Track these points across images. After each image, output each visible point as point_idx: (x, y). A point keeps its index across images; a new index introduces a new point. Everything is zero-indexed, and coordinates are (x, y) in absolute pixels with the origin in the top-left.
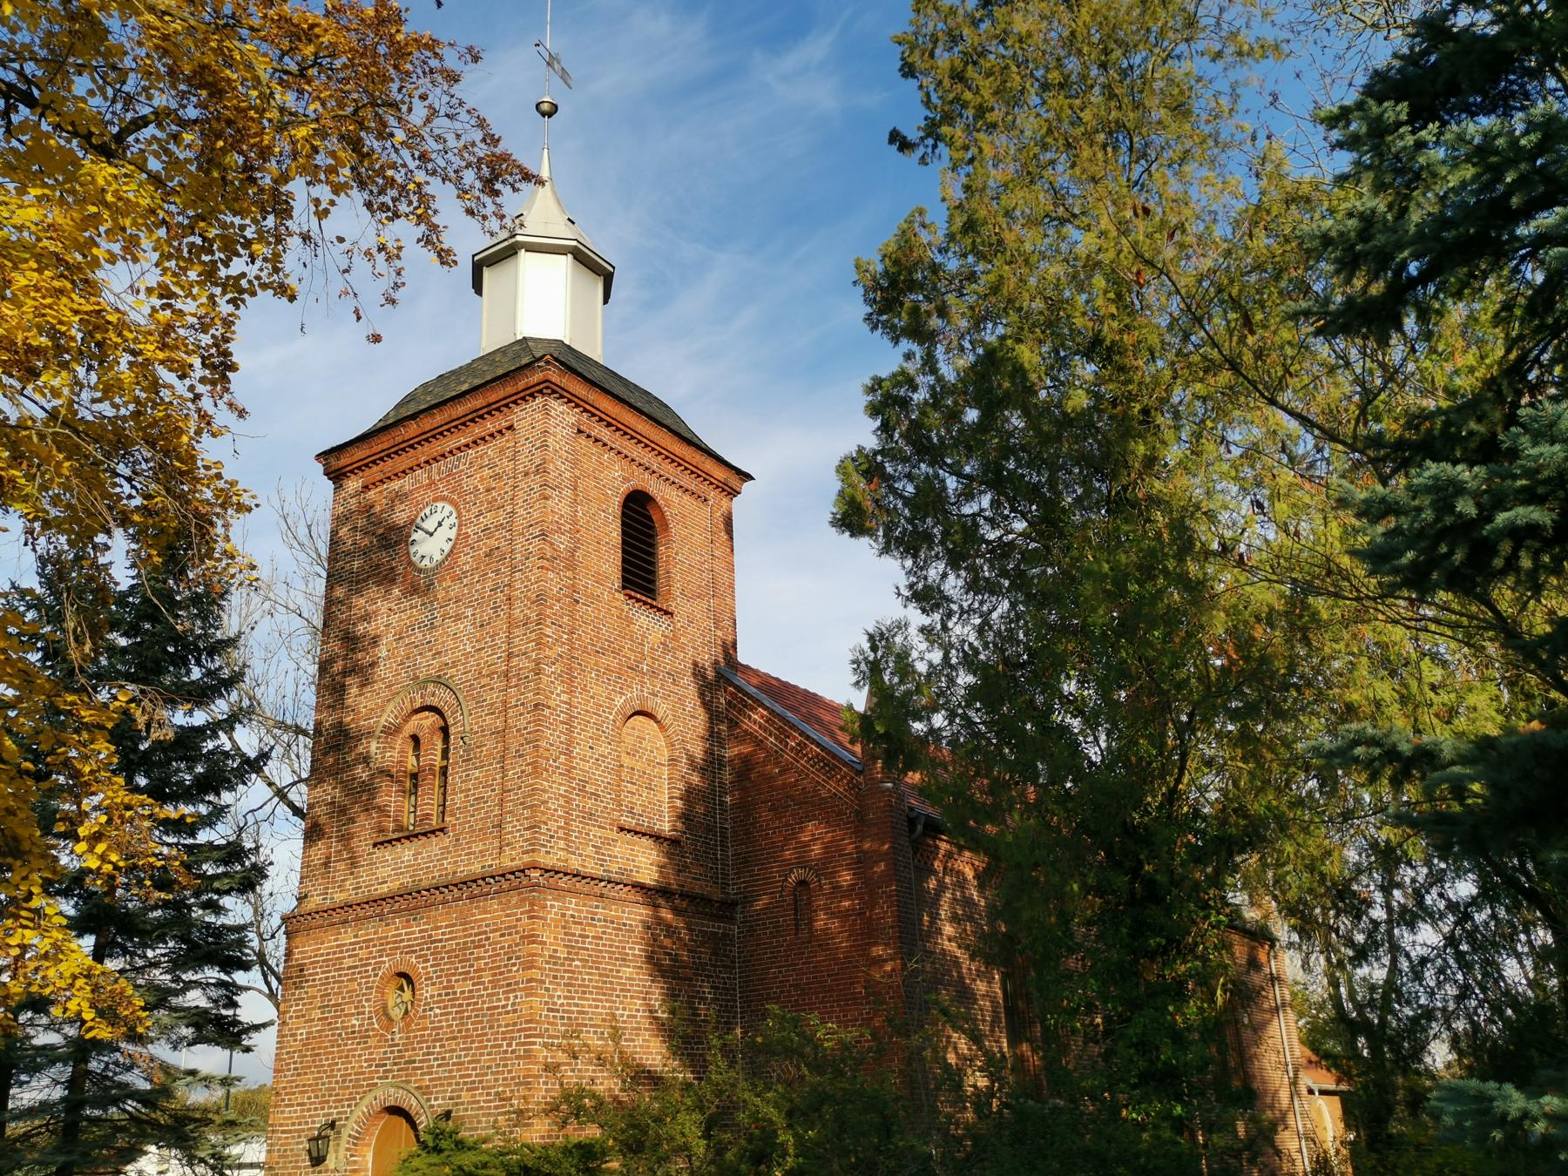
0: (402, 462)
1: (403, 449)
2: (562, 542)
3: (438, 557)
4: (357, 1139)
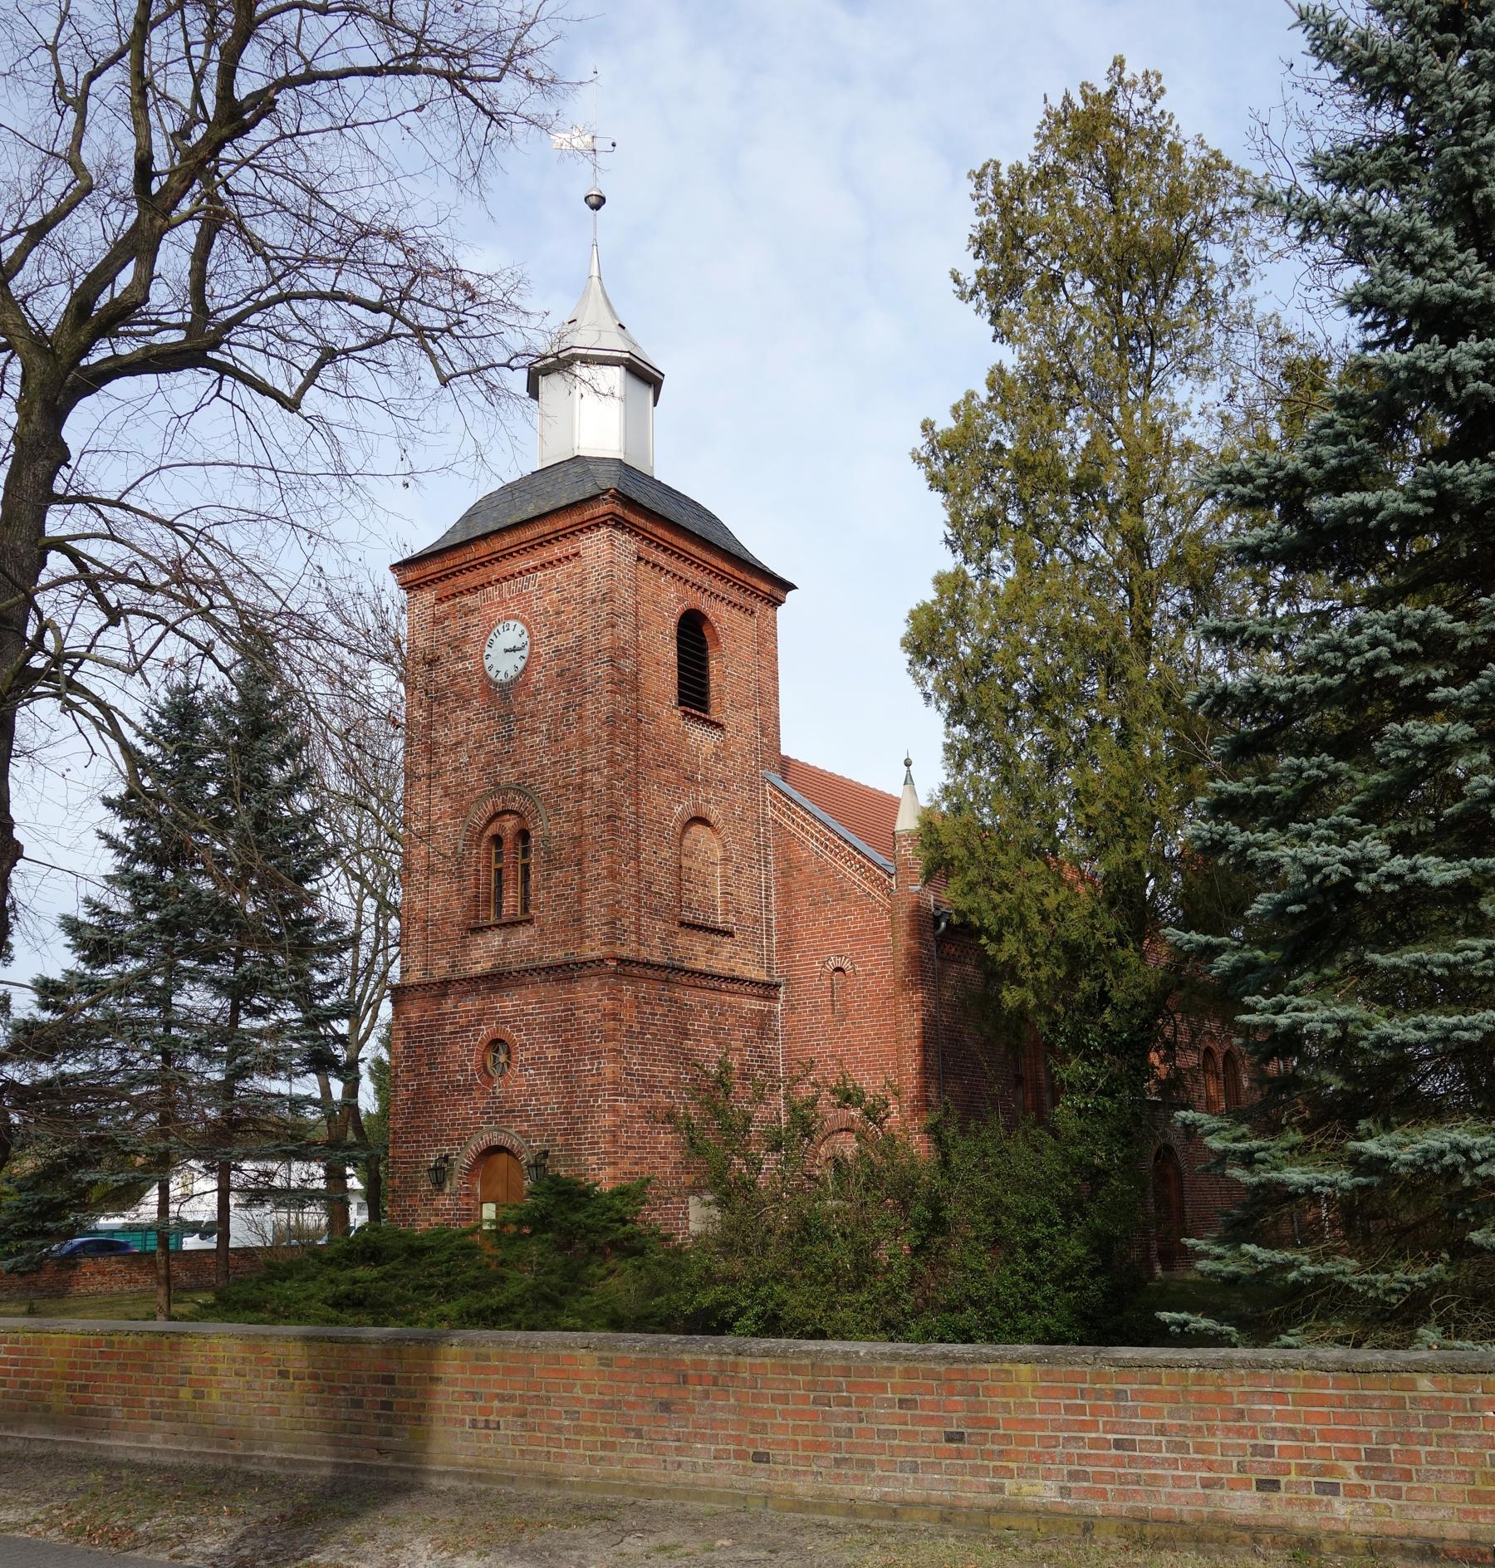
1: (474, 566)
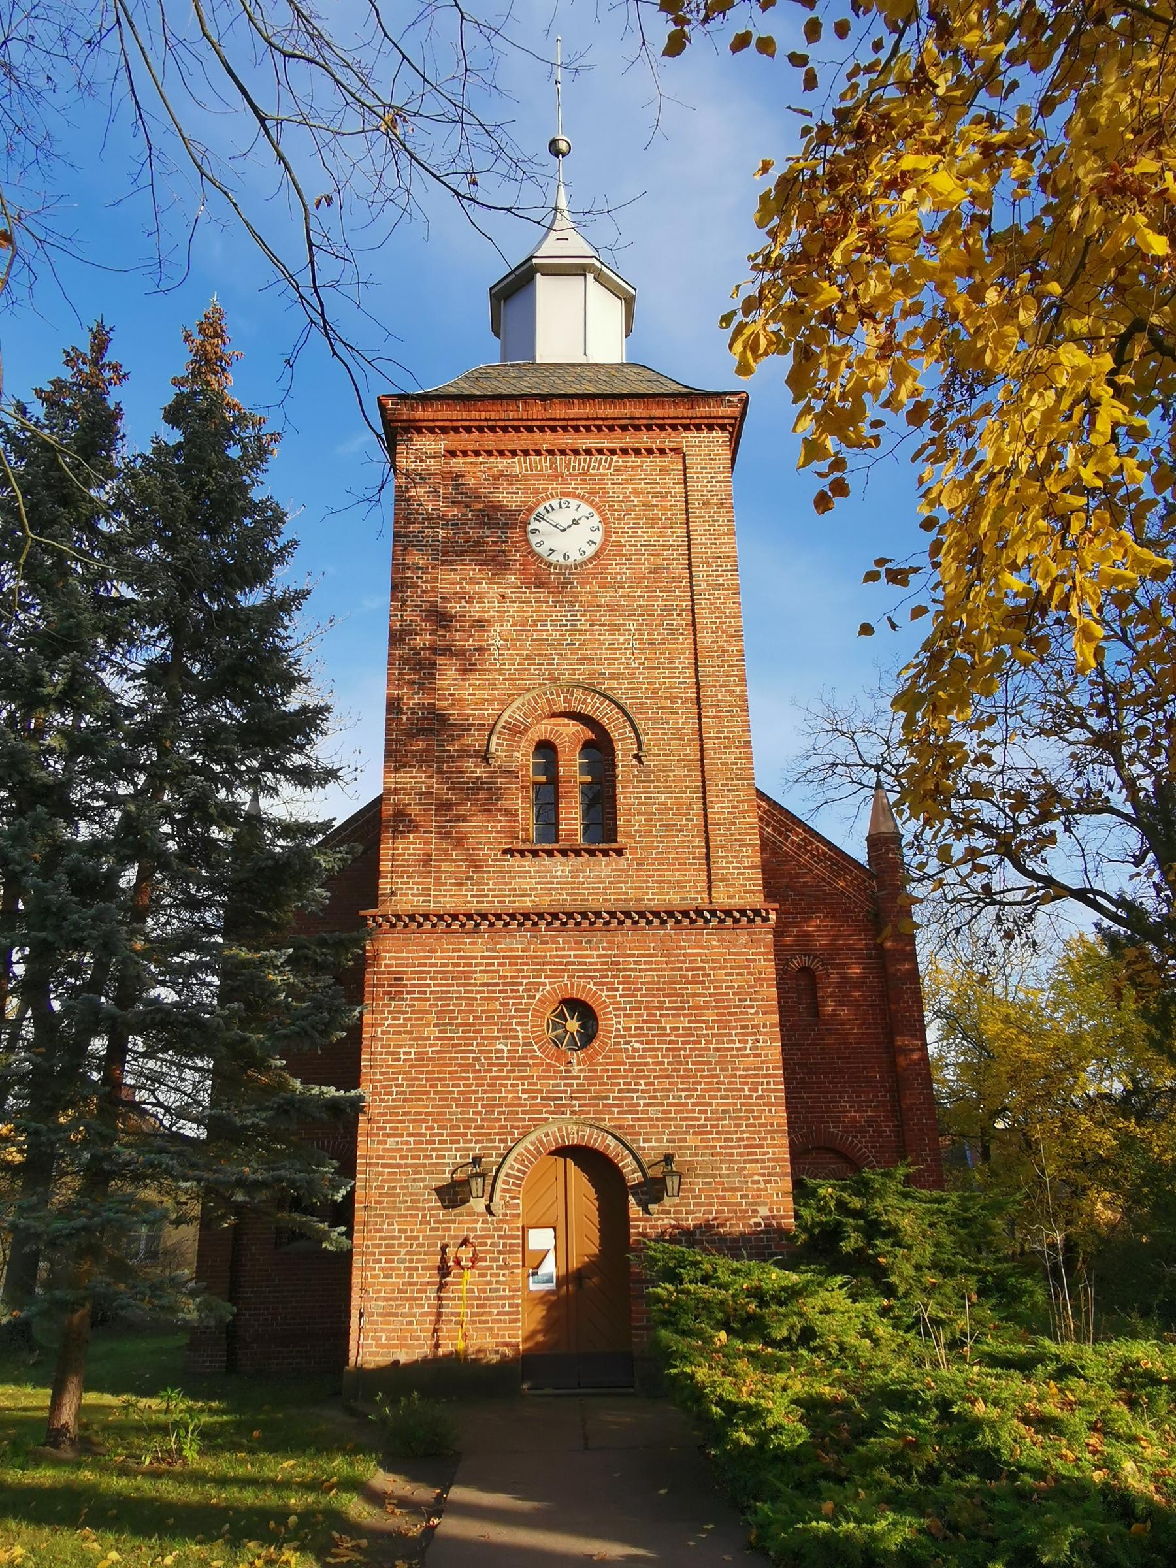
0: (521, 441)
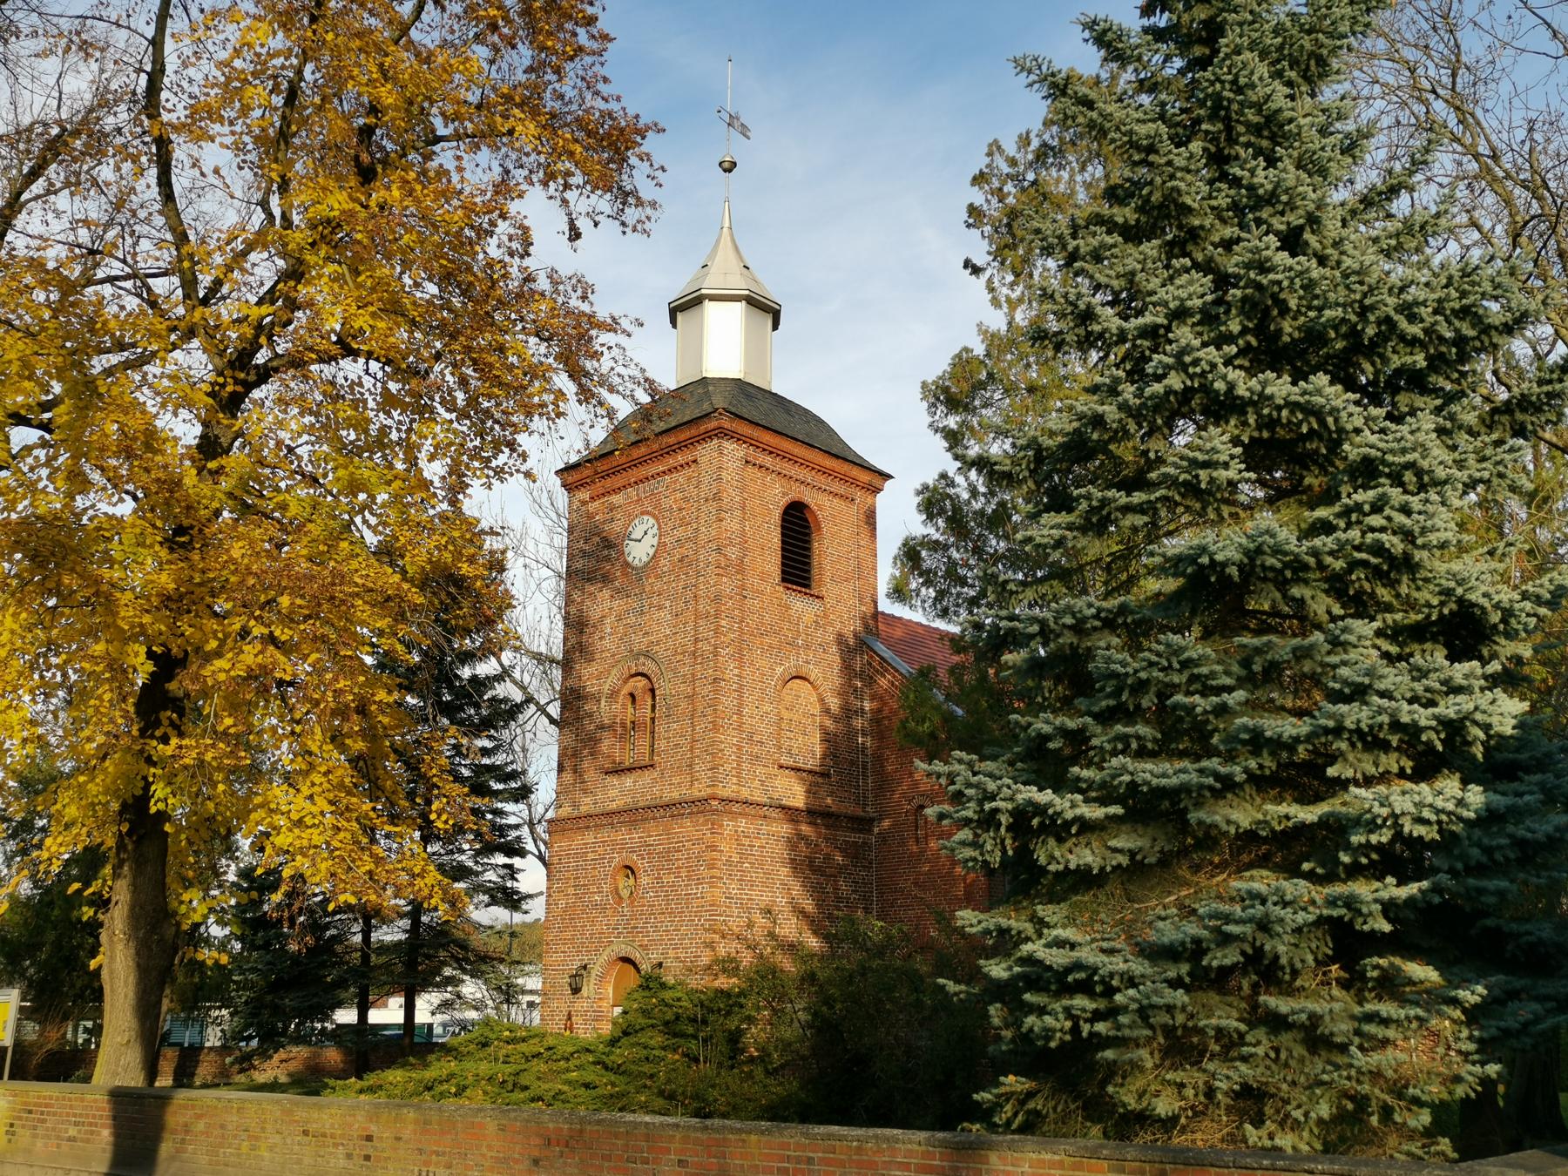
2: (733, 553)
3: (645, 559)
4: (602, 978)
